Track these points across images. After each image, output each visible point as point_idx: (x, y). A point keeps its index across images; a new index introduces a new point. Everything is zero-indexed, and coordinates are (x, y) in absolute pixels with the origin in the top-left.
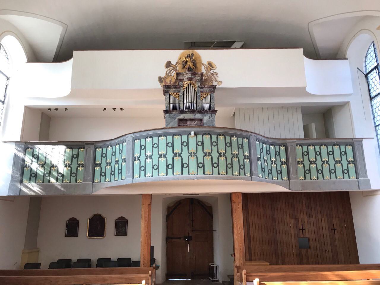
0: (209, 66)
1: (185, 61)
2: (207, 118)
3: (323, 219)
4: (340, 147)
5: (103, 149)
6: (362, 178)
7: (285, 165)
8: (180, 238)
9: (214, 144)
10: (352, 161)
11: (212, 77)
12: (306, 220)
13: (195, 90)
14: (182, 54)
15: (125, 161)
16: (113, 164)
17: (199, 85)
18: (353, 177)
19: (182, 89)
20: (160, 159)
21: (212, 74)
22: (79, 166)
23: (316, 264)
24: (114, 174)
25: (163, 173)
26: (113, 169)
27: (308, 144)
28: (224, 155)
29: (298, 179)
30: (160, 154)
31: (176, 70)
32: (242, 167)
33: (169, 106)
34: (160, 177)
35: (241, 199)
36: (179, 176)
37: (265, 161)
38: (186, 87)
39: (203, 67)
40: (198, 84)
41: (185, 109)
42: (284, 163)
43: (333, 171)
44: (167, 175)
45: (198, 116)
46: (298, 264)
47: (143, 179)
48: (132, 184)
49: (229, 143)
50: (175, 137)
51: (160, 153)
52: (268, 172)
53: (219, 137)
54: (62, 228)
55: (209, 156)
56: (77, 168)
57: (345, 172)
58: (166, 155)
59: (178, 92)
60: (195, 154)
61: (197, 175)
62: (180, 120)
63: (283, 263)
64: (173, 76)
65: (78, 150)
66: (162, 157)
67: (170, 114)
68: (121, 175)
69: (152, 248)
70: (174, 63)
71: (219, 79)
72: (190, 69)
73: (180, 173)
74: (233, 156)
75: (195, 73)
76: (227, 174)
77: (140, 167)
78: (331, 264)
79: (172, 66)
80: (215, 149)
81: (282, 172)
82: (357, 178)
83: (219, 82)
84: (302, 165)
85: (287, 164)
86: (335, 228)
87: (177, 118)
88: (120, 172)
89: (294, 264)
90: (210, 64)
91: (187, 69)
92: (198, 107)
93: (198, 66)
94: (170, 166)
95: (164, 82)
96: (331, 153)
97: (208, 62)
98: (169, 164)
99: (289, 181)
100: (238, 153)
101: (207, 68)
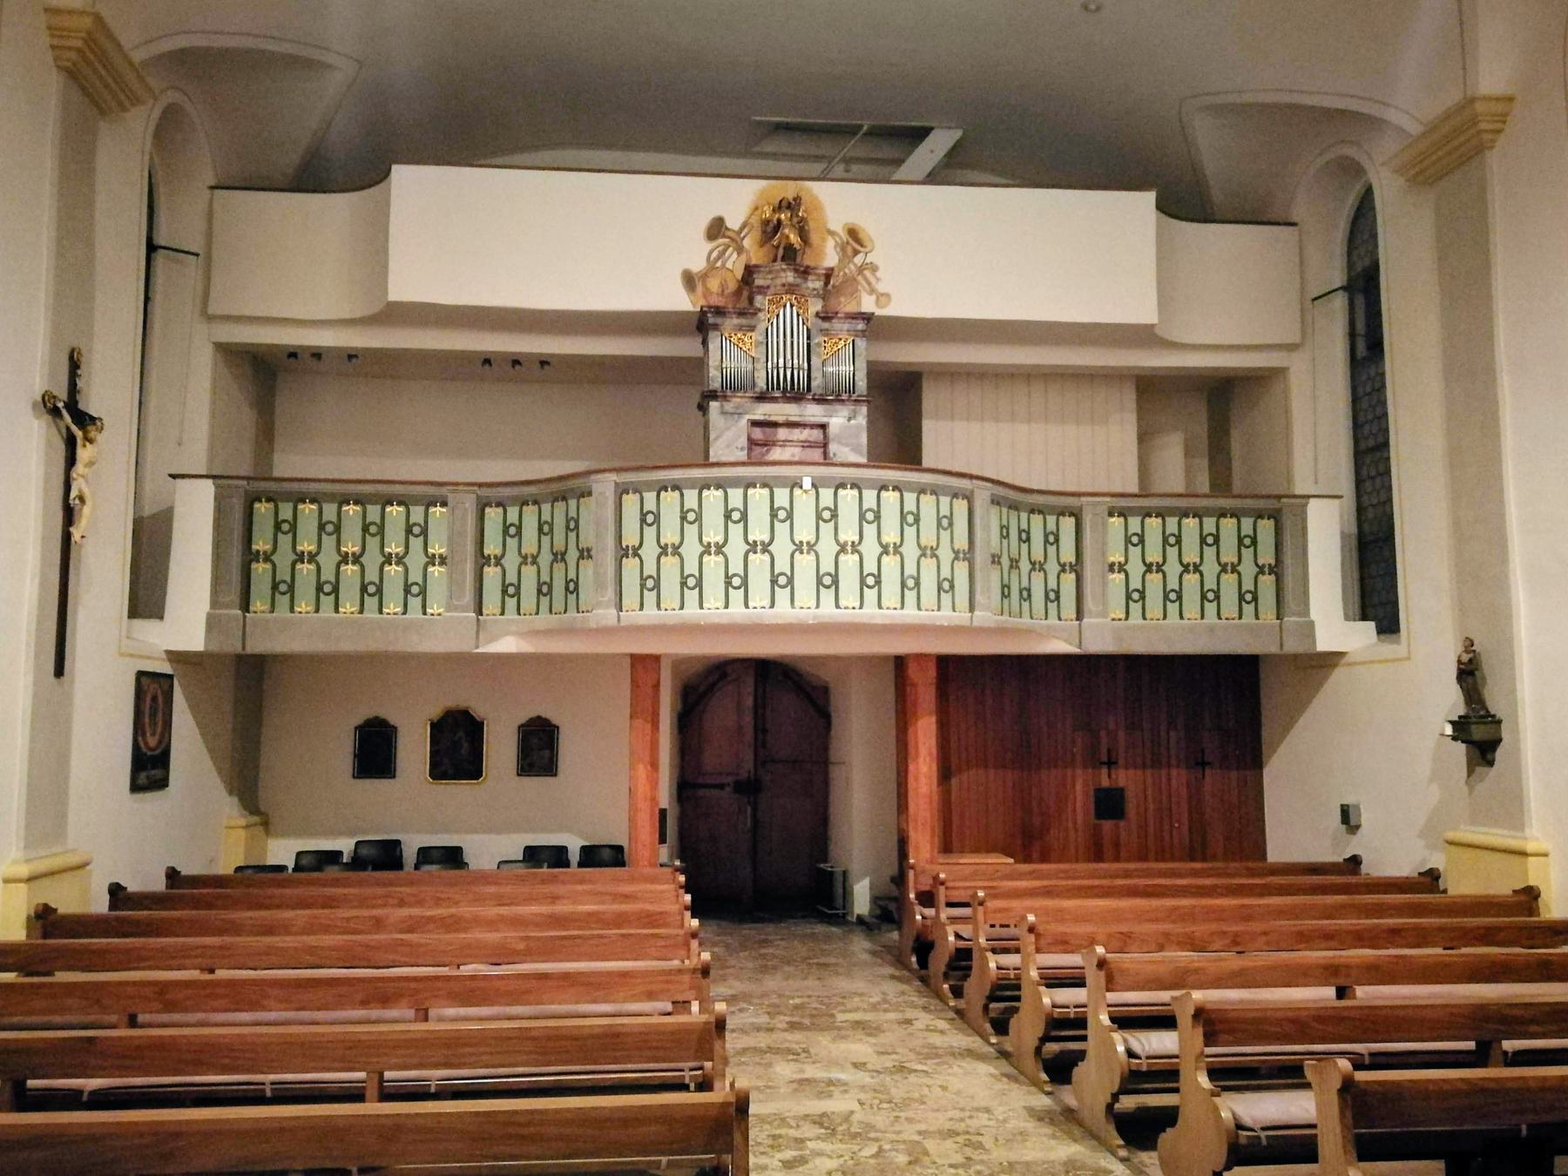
0: (850, 240)
3: (1172, 734)
8: (721, 787)
9: (870, 516)
10: (1270, 565)
12: (1121, 735)
13: (804, 324)
14: (763, 192)
15: (590, 557)
20: (706, 558)
21: (861, 270)
22: (431, 560)
26: (545, 577)
27: (1144, 512)
28: (897, 549)
32: (946, 585)
37: (1014, 564)
38: (778, 316)
41: (773, 388)
42: (1067, 568)
43: (1211, 596)
45: (813, 412)
46: (1089, 861)
47: (650, 614)
50: (751, 491)
55: (852, 553)
56: (425, 569)
57: (1249, 597)
58: (724, 545)
59: (748, 331)
60: (811, 546)
63: (1044, 859)
64: (732, 271)
67: (724, 403)
70: (733, 223)
71: (881, 288)
73: (767, 602)
74: (924, 552)
76: (902, 608)
78: (1181, 860)
79: (729, 233)
80: (870, 530)
82: (1278, 619)
83: (882, 299)
84: (1122, 576)
85: (1076, 571)
86: (1206, 760)
89: (1077, 861)
90: (853, 233)
92: (814, 384)
93: (814, 238)
94: (736, 581)
95: (700, 289)
96: (1210, 540)
98: (735, 575)
100: (938, 546)
101: (842, 248)
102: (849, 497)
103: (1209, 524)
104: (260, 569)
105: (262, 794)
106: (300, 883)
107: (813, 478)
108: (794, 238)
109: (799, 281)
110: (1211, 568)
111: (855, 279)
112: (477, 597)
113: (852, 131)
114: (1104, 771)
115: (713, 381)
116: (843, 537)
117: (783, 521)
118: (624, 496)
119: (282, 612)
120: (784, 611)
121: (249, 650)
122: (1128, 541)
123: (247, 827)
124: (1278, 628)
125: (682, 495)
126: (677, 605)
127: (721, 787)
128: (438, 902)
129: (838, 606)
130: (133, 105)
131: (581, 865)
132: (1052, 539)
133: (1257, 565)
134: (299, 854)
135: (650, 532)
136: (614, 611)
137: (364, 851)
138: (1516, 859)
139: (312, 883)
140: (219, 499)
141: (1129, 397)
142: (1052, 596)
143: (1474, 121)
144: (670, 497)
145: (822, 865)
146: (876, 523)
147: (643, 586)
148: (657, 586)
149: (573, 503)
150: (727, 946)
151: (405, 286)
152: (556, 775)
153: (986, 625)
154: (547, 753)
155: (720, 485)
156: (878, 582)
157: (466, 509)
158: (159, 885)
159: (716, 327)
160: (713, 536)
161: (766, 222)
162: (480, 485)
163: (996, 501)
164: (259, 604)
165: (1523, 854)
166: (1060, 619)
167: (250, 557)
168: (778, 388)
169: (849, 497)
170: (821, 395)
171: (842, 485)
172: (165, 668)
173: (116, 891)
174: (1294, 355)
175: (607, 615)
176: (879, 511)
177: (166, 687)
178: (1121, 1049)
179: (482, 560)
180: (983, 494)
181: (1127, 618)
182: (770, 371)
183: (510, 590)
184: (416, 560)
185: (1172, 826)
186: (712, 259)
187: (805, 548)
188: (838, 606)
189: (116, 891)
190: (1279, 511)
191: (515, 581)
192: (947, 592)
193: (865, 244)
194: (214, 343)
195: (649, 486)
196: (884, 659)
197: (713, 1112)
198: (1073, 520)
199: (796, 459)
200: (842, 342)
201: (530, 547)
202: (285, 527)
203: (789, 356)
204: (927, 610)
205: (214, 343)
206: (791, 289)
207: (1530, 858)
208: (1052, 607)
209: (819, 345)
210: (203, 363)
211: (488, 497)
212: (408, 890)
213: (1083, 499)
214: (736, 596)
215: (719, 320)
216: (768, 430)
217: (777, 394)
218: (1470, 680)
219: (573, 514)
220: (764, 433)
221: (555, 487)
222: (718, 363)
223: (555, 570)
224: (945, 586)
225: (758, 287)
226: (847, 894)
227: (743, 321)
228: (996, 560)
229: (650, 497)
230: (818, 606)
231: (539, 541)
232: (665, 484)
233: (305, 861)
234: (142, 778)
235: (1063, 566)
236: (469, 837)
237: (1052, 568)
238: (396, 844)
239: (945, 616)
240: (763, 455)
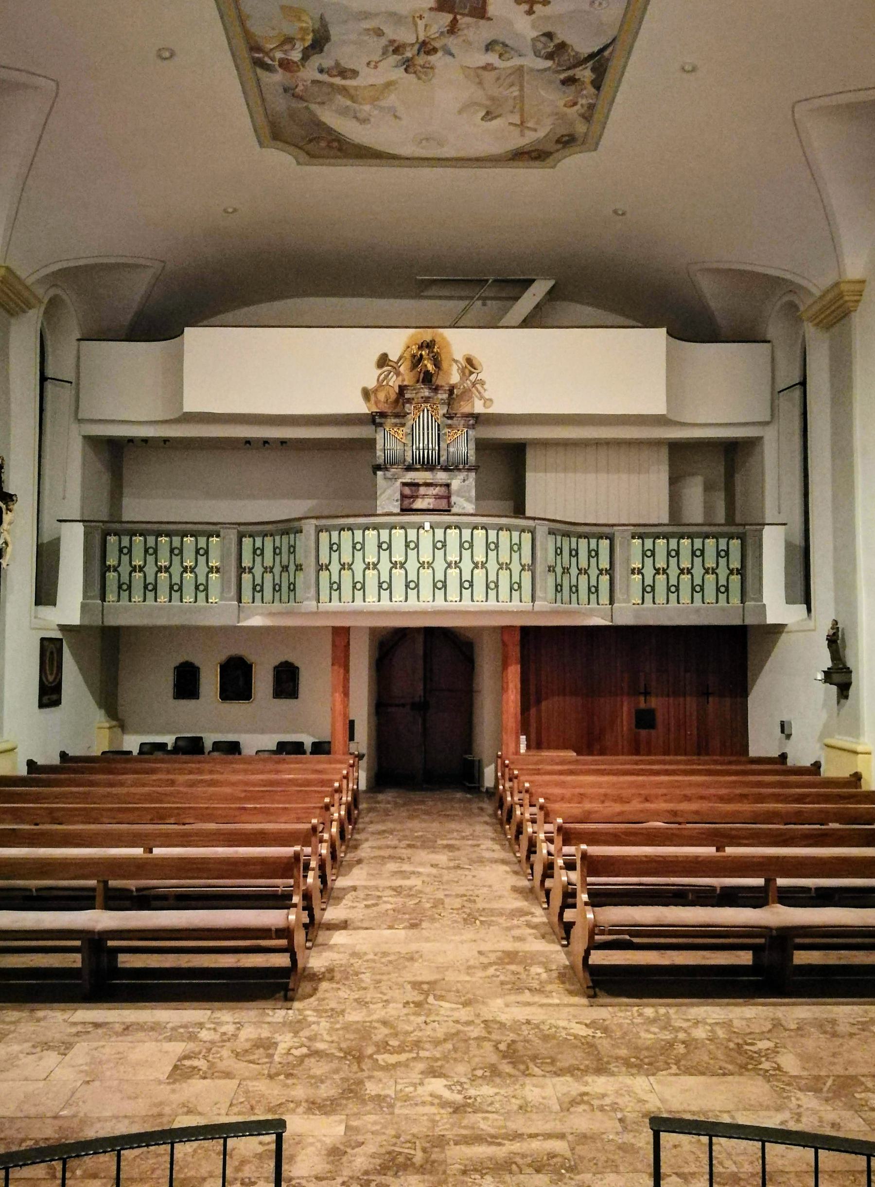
0: (468, 366)
2: (459, 481)
4: (717, 542)
6: (753, 603)
8: (403, 705)
9: (466, 545)
15: (301, 569)
17: (445, 411)
18: (735, 600)
20: (367, 572)
21: (474, 384)
22: (211, 570)
23: (664, 754)
24: (280, 590)
25: (371, 597)
29: (629, 602)
34: (366, 603)
35: (517, 637)
39: (455, 367)
44: (379, 601)
45: (441, 476)
47: (335, 605)
50: (393, 531)
51: (367, 560)
53: (475, 532)
54: (167, 682)
57: (723, 590)
63: (602, 753)
65: (208, 539)
69: (352, 723)
70: (394, 357)
71: (487, 395)
79: (391, 363)
83: (488, 402)
87: (400, 480)
90: (469, 361)
92: (442, 459)
93: (445, 365)
94: (385, 586)
95: (373, 398)
101: (462, 371)
103: (698, 543)
104: (111, 576)
105: (120, 708)
106: (141, 761)
108: (430, 367)
109: (432, 394)
110: (698, 571)
113: (482, 282)
114: (642, 699)
116: (449, 559)
117: (413, 549)
119: (124, 602)
120: (413, 603)
121: (106, 623)
122: (644, 554)
123: (110, 728)
124: (741, 610)
127: (403, 705)
128: (211, 772)
129: (446, 600)
130: (30, 309)
131: (311, 753)
132: (594, 554)
133: (728, 568)
134: (142, 744)
135: (335, 555)
136: (314, 603)
137: (180, 743)
138: (852, 755)
139: (146, 761)
140: (86, 534)
141: (664, 452)
143: (841, 295)
144: (346, 535)
147: (331, 588)
148: (339, 588)
149: (292, 536)
150: (396, 803)
151: (190, 406)
152: (297, 698)
153: (544, 609)
155: (376, 527)
156: (471, 586)
157: (231, 539)
158: (56, 761)
159: (381, 425)
160: (371, 559)
161: (414, 356)
162: (239, 524)
163: (551, 532)
164: (111, 597)
165: (856, 753)
166: (598, 604)
167: (105, 569)
171: (449, 527)
172: (58, 635)
173: (31, 764)
174: (767, 428)
175: (311, 605)
177: (58, 646)
178: (545, 851)
179: (241, 570)
180: (542, 530)
181: (643, 603)
183: (258, 588)
184: (202, 569)
185: (686, 734)
187: (426, 565)
188: (446, 600)
189: (31, 764)
190: (744, 534)
194: (85, 437)
197: (286, 861)
198: (608, 541)
199: (431, 507)
201: (268, 562)
202: (125, 551)
205: (85, 437)
206: (426, 400)
207: (860, 756)
208: (593, 597)
209: (445, 434)
210: (76, 450)
211: (246, 530)
212: (193, 765)
213: (615, 528)
214: (385, 594)
215: (382, 420)
216: (413, 488)
218: (834, 645)
219: (292, 543)
220: (411, 490)
221: (281, 526)
222: (382, 447)
224: (515, 587)
227: (397, 421)
228: (551, 569)
229: (335, 534)
233: (145, 749)
234: (45, 700)
235: (601, 571)
238: (200, 739)
239: (515, 605)
240: (410, 504)
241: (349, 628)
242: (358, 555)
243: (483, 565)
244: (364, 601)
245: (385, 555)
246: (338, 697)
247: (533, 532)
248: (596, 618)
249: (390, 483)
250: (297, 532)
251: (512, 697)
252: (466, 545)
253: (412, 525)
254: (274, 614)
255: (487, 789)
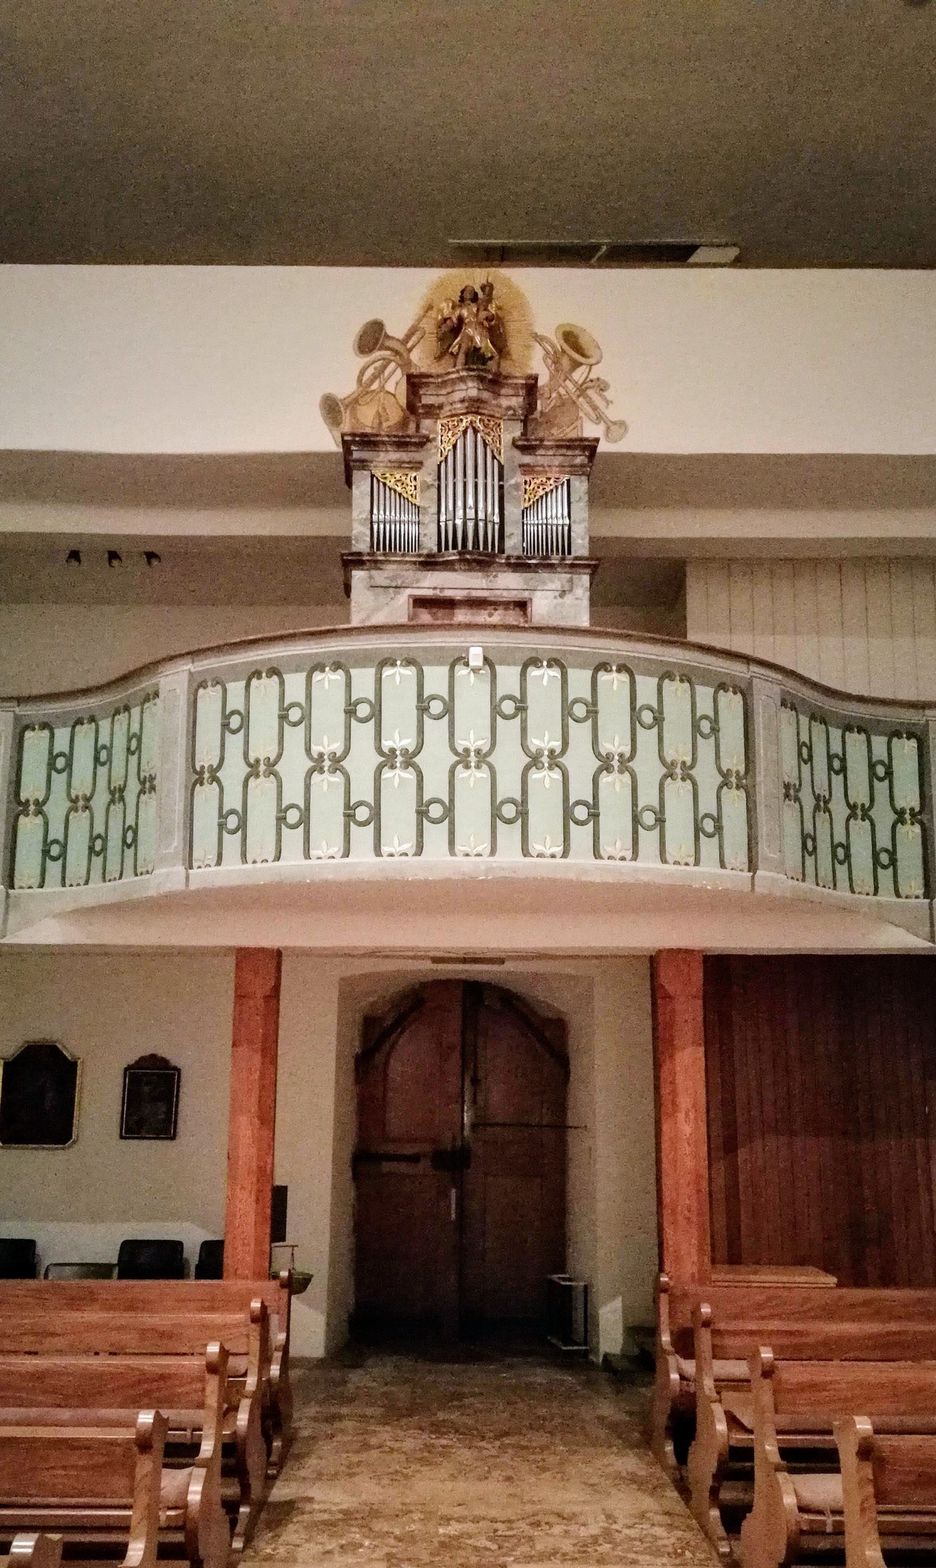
0: (566, 347)
1: (450, 318)
5: (56, 731)
7: (912, 824)
8: (414, 1159)
11: (581, 399)
13: (494, 457)
14: (440, 285)
16: (101, 800)
17: (518, 434)
19: (436, 454)
21: (582, 390)
26: (99, 829)
30: (316, 756)
31: (406, 364)
32: (709, 825)
33: (368, 532)
35: (698, 976)
36: (404, 858)
37: (822, 804)
38: (455, 446)
40: (511, 432)
42: (907, 816)
44: (346, 854)
48: (183, 892)
49: (650, 708)
50: (387, 672)
51: (316, 749)
52: (834, 855)
53: (603, 677)
55: (550, 768)
61: (491, 859)
62: (420, 602)
63: (887, 1280)
64: (394, 396)
66: (326, 769)
67: (373, 572)
68: (136, 854)
69: (280, 1196)
70: (396, 329)
71: (612, 414)
72: (474, 357)
75: (498, 374)
77: (221, 815)
79: (388, 343)
81: (896, 860)
85: (922, 824)
87: (409, 592)
88: (129, 841)
90: (571, 338)
91: (461, 358)
92: (509, 543)
93: (515, 345)
94: (362, 814)
97: (560, 326)
99: (927, 901)
100: (694, 759)
101: (555, 359)
102: (546, 678)
107: (485, 649)
108: (480, 340)
109: (486, 395)
111: (574, 402)
112: (8, 862)
115: (357, 541)
116: (535, 743)
117: (438, 717)
118: (201, 691)
125: (282, 683)
126: (271, 853)
127: (414, 1159)
136: (181, 869)
142: (884, 858)
144: (265, 688)
145: (555, 1277)
146: (589, 722)
148: (243, 825)
152: (173, 1138)
154: (162, 1107)
156: (594, 816)
159: (363, 464)
162: (20, 700)
168: (455, 546)
169: (546, 678)
170: (518, 558)
176: (595, 703)
182: (443, 525)
186: (365, 378)
187: (473, 759)
188: (526, 853)
191: (61, 838)
192: (710, 836)
193: (589, 353)
195: (234, 672)
196: (628, 958)
198: (913, 743)
200: (552, 482)
203: (470, 472)
204: (676, 863)
208: (885, 876)
209: (517, 486)
214: (362, 836)
217: (452, 555)
222: (366, 515)
223: (112, 813)
225: (424, 406)
226: (590, 1320)
228: (790, 792)
230: (493, 852)
231: (95, 774)
232: (259, 667)
236: (53, 1227)
237: (883, 816)
241: (277, 955)
242: (294, 737)
243: (625, 763)
244: (307, 856)
245: (363, 733)
246: (247, 1128)
247: (745, 693)
248: (892, 929)
249: (382, 599)
250: (147, 699)
251: (687, 1129)
252: (580, 710)
253: (438, 656)
254: (91, 910)
255: (606, 1356)
